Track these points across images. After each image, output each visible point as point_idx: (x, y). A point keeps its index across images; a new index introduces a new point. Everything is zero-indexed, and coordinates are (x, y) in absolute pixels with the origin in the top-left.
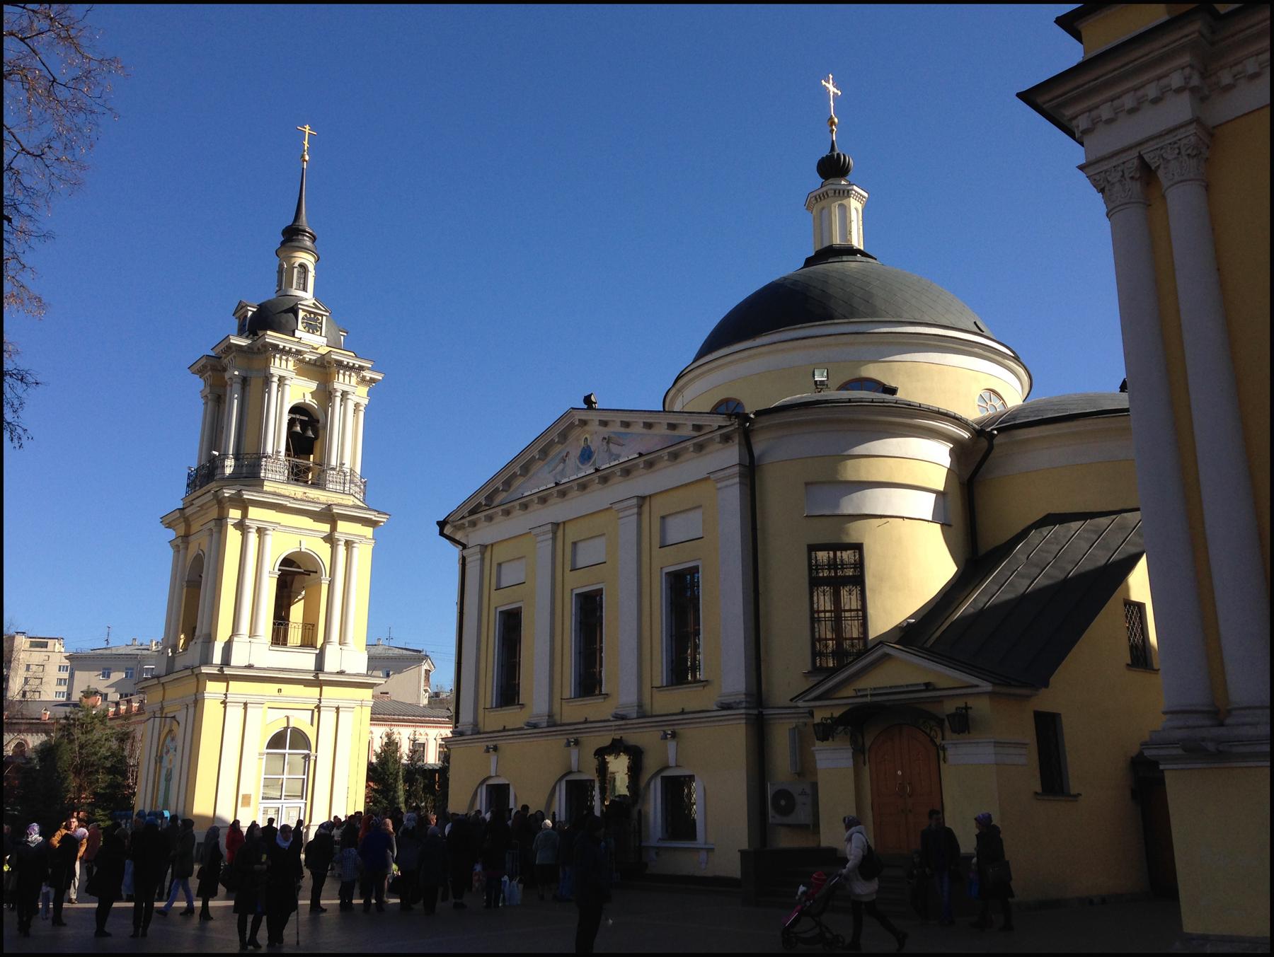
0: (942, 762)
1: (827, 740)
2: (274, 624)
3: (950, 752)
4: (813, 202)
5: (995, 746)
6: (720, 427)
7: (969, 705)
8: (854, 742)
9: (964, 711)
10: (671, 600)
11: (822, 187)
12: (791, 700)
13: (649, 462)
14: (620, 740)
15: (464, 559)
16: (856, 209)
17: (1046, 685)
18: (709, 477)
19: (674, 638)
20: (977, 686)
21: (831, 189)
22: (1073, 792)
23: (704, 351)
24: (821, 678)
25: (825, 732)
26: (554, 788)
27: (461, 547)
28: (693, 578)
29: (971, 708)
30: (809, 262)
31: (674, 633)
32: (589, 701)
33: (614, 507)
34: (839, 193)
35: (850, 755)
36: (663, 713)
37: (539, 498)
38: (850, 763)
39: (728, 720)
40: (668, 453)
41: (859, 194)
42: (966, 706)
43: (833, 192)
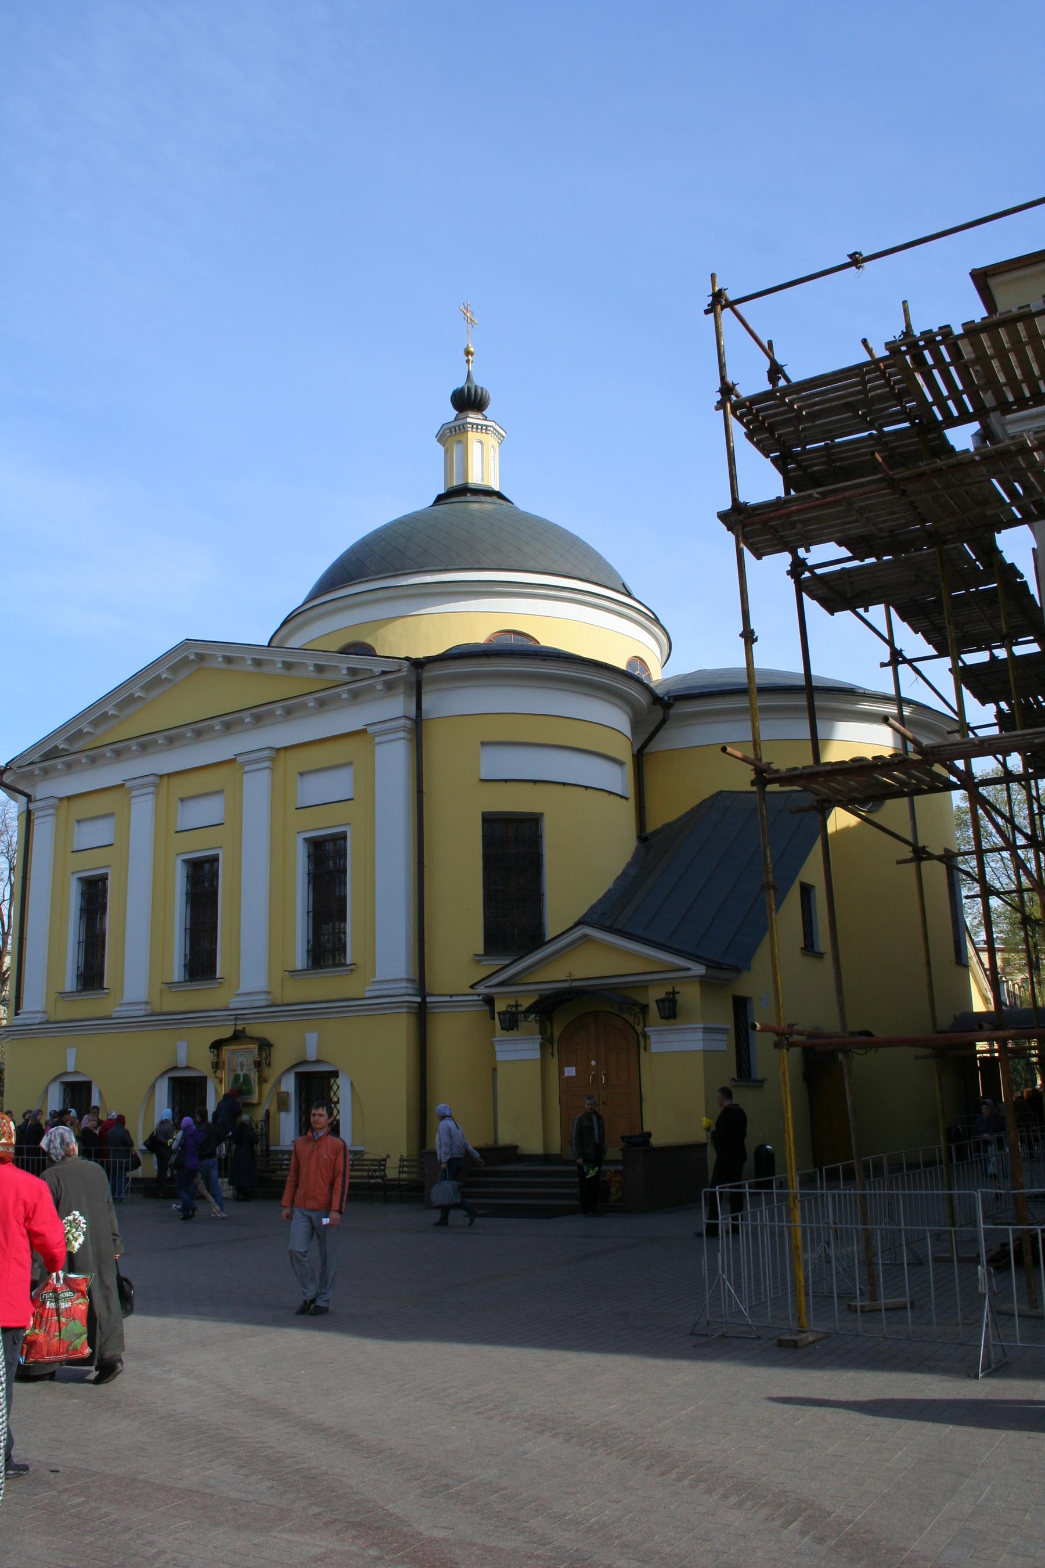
0: (642, 1051)
1: (513, 1029)
2: (1043, 616)
3: (654, 1038)
4: (448, 435)
5: (703, 1032)
6: (384, 673)
7: (676, 990)
8: (542, 1032)
9: (514, 1009)
10: (309, 870)
11: (455, 420)
12: (472, 987)
13: (291, 710)
14: (243, 1031)
15: (29, 813)
16: (493, 447)
17: (749, 968)
18: (366, 729)
19: (311, 914)
20: (689, 969)
21: (447, 429)
22: (759, 1077)
23: (315, 594)
24: (507, 962)
25: (511, 1021)
26: (153, 1087)
27: (25, 799)
28: (212, 866)
29: (678, 993)
30: (440, 499)
31: (311, 909)
32: (91, 996)
33: (238, 759)
34: (455, 430)
35: (538, 1046)
36: (294, 1001)
37: (112, 750)
38: (537, 1055)
39: (157, 1025)
40: (383, 681)
41: (497, 431)
42: (517, 1003)
43: (448, 431)
